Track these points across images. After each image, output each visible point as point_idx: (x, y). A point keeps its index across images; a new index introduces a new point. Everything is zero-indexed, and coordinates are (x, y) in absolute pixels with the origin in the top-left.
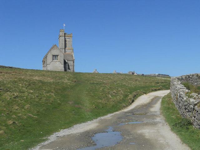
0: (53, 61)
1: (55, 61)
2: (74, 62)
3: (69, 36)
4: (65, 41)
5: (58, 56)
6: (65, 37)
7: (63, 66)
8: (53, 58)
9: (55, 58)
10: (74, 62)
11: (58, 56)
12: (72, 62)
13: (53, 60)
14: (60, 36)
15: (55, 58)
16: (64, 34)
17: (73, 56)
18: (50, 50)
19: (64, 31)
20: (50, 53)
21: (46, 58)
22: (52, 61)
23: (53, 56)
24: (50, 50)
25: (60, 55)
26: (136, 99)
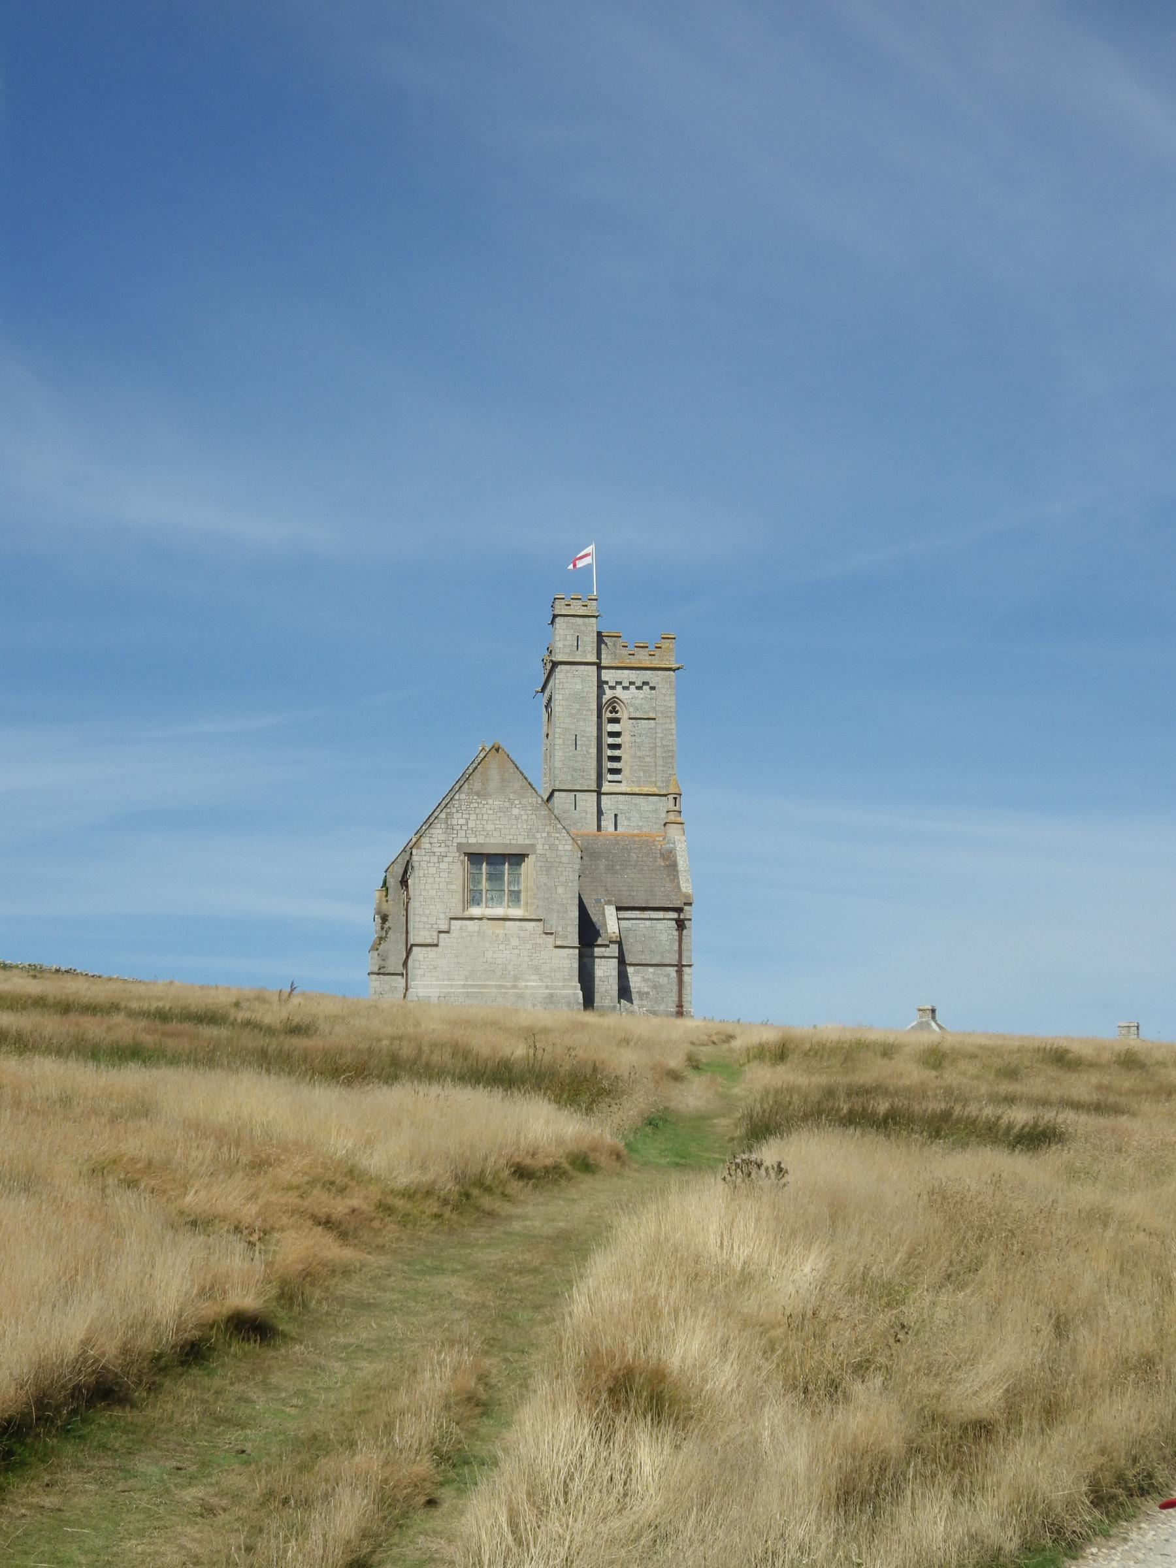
0: (475, 911)
1: (499, 911)
2: (681, 925)
3: (643, 658)
4: (607, 710)
5: (517, 859)
6: (599, 794)
7: (569, 960)
8: (474, 879)
9: (495, 878)
10: (681, 925)
11: (517, 859)
12: (664, 927)
13: (474, 898)
14: (555, 665)
15: (495, 878)
16: (593, 637)
17: (682, 863)
18: (446, 803)
19: (593, 607)
20: (438, 832)
21: (404, 882)
22: (455, 904)
23: (475, 858)
24: (446, 803)
25: (540, 848)
26: (964, 1145)
